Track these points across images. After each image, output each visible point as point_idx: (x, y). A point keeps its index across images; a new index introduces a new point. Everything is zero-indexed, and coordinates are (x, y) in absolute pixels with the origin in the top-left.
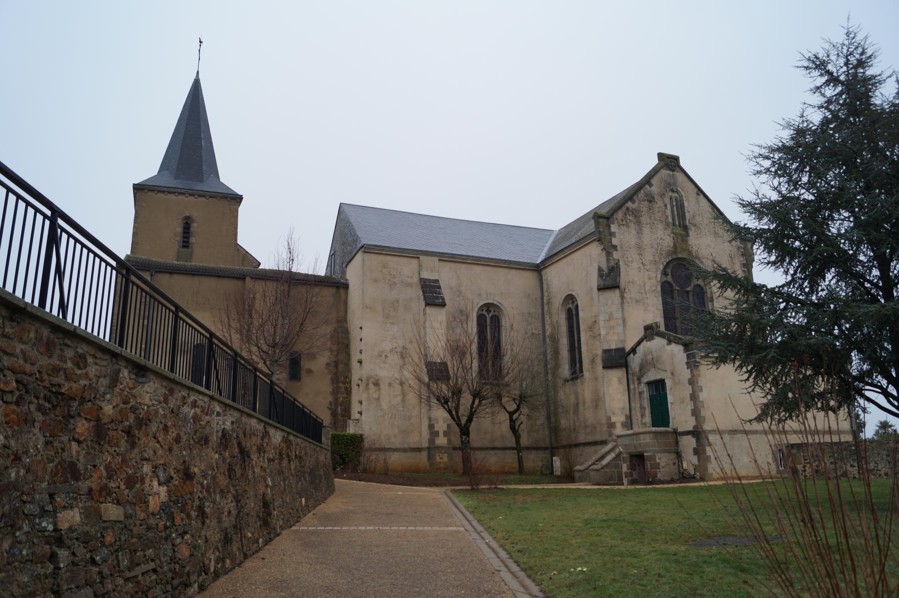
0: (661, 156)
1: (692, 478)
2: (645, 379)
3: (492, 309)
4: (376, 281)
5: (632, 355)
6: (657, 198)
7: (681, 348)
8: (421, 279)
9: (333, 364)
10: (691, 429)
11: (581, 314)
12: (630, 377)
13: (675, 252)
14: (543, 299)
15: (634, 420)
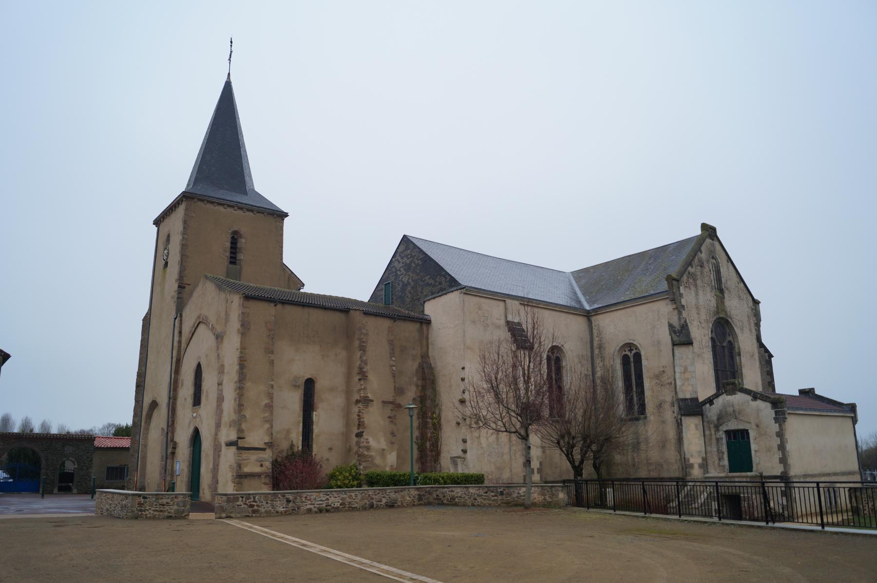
0: (704, 226)
1: (781, 518)
2: (724, 428)
3: (556, 351)
4: (474, 322)
5: (708, 405)
6: (705, 264)
7: (769, 405)
8: (508, 323)
9: (419, 399)
10: (779, 474)
11: (644, 362)
12: (705, 424)
13: (718, 313)
14: (594, 346)
15: (710, 462)
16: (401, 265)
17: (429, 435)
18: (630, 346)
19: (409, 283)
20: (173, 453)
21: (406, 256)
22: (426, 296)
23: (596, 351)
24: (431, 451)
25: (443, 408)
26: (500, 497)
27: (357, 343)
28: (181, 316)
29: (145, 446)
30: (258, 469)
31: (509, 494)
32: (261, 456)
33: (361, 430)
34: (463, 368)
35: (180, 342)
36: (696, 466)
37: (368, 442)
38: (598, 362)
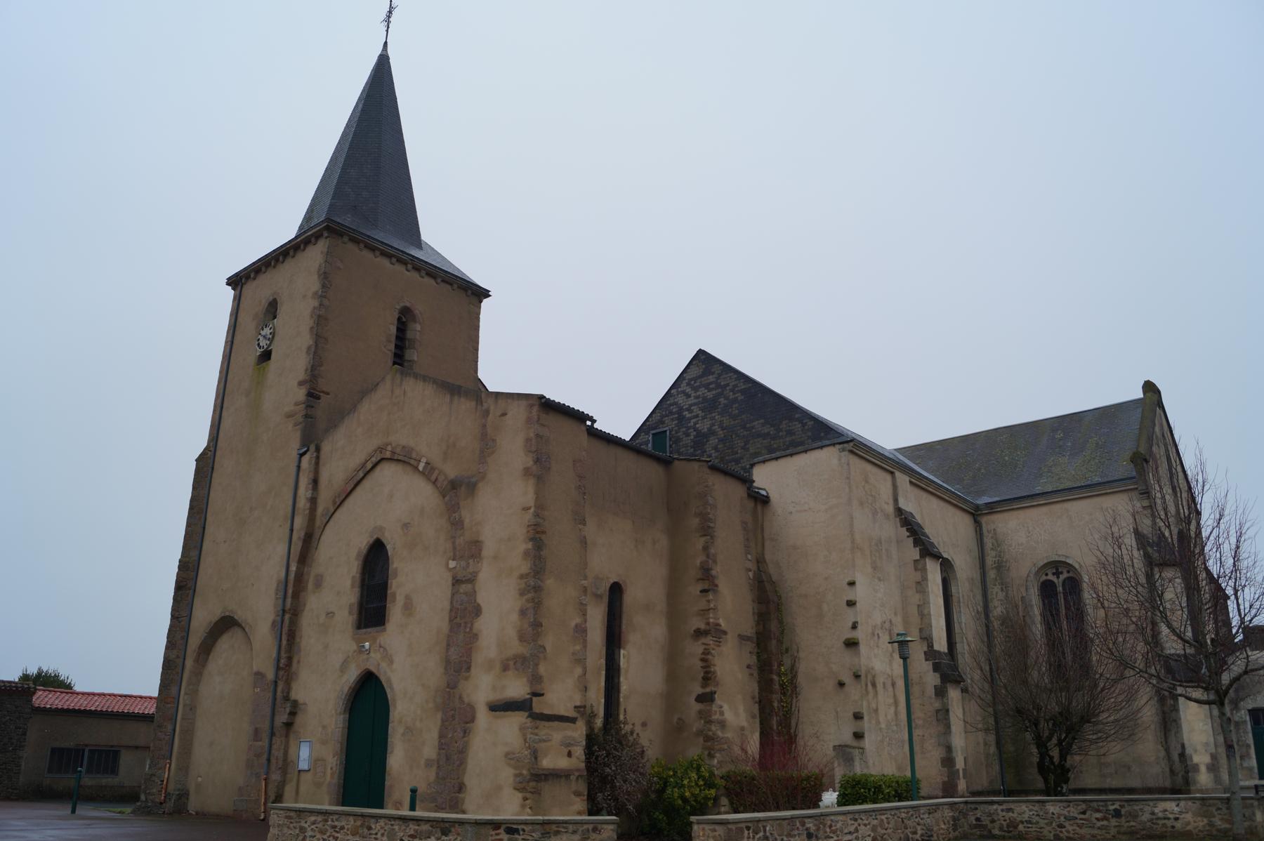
16: (692, 401)
17: (776, 704)
18: (1057, 566)
19: (712, 432)
20: (289, 725)
21: (707, 386)
22: (757, 454)
23: (992, 574)
24: (779, 733)
25: (802, 655)
26: (1114, 822)
27: (695, 522)
28: (318, 450)
29: (192, 708)
30: (563, 763)
31: (1134, 816)
32: (569, 733)
33: (708, 690)
34: (852, 584)
35: (313, 501)
36: (1203, 769)
37: (722, 713)
38: (996, 592)
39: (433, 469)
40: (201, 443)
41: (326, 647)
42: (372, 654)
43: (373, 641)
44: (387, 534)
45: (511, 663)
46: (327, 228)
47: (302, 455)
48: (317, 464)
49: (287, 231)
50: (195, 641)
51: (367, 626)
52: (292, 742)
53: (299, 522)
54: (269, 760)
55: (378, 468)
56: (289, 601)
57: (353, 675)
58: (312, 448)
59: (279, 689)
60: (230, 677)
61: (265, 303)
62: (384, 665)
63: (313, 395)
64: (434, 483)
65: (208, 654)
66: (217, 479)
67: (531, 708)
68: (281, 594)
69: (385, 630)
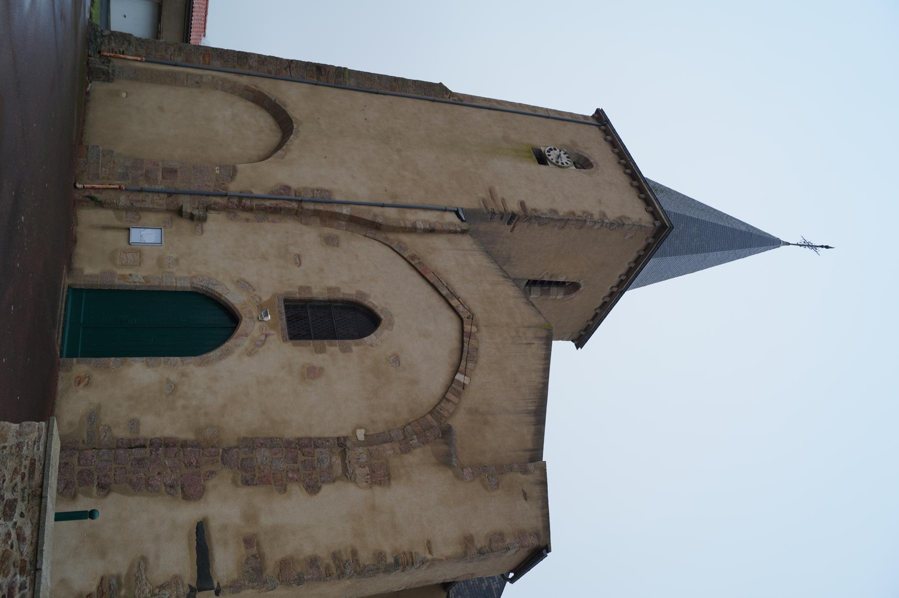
20: (180, 212)
28: (463, 232)
29: (198, 83)
35: (413, 230)
39: (458, 394)
40: (455, 86)
41: (264, 258)
42: (258, 324)
43: (272, 325)
44: (386, 333)
45: (254, 551)
46: (663, 227)
47: (457, 213)
48: (450, 232)
49: (648, 171)
50: (265, 86)
51: (286, 307)
52: (161, 216)
53: (392, 214)
54: (141, 191)
55: (452, 314)
56: (311, 206)
57: (235, 298)
58: (465, 226)
59: (218, 200)
60: (231, 125)
61: (587, 153)
62: (246, 343)
63: (512, 218)
64: (444, 397)
65: (253, 101)
66: (425, 106)
67: (201, 589)
68: (318, 197)
69: (285, 341)
